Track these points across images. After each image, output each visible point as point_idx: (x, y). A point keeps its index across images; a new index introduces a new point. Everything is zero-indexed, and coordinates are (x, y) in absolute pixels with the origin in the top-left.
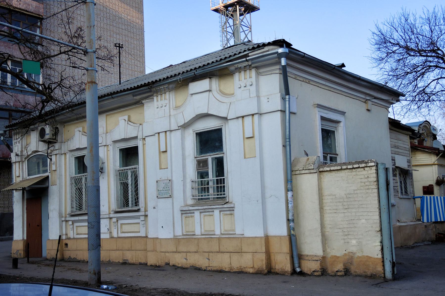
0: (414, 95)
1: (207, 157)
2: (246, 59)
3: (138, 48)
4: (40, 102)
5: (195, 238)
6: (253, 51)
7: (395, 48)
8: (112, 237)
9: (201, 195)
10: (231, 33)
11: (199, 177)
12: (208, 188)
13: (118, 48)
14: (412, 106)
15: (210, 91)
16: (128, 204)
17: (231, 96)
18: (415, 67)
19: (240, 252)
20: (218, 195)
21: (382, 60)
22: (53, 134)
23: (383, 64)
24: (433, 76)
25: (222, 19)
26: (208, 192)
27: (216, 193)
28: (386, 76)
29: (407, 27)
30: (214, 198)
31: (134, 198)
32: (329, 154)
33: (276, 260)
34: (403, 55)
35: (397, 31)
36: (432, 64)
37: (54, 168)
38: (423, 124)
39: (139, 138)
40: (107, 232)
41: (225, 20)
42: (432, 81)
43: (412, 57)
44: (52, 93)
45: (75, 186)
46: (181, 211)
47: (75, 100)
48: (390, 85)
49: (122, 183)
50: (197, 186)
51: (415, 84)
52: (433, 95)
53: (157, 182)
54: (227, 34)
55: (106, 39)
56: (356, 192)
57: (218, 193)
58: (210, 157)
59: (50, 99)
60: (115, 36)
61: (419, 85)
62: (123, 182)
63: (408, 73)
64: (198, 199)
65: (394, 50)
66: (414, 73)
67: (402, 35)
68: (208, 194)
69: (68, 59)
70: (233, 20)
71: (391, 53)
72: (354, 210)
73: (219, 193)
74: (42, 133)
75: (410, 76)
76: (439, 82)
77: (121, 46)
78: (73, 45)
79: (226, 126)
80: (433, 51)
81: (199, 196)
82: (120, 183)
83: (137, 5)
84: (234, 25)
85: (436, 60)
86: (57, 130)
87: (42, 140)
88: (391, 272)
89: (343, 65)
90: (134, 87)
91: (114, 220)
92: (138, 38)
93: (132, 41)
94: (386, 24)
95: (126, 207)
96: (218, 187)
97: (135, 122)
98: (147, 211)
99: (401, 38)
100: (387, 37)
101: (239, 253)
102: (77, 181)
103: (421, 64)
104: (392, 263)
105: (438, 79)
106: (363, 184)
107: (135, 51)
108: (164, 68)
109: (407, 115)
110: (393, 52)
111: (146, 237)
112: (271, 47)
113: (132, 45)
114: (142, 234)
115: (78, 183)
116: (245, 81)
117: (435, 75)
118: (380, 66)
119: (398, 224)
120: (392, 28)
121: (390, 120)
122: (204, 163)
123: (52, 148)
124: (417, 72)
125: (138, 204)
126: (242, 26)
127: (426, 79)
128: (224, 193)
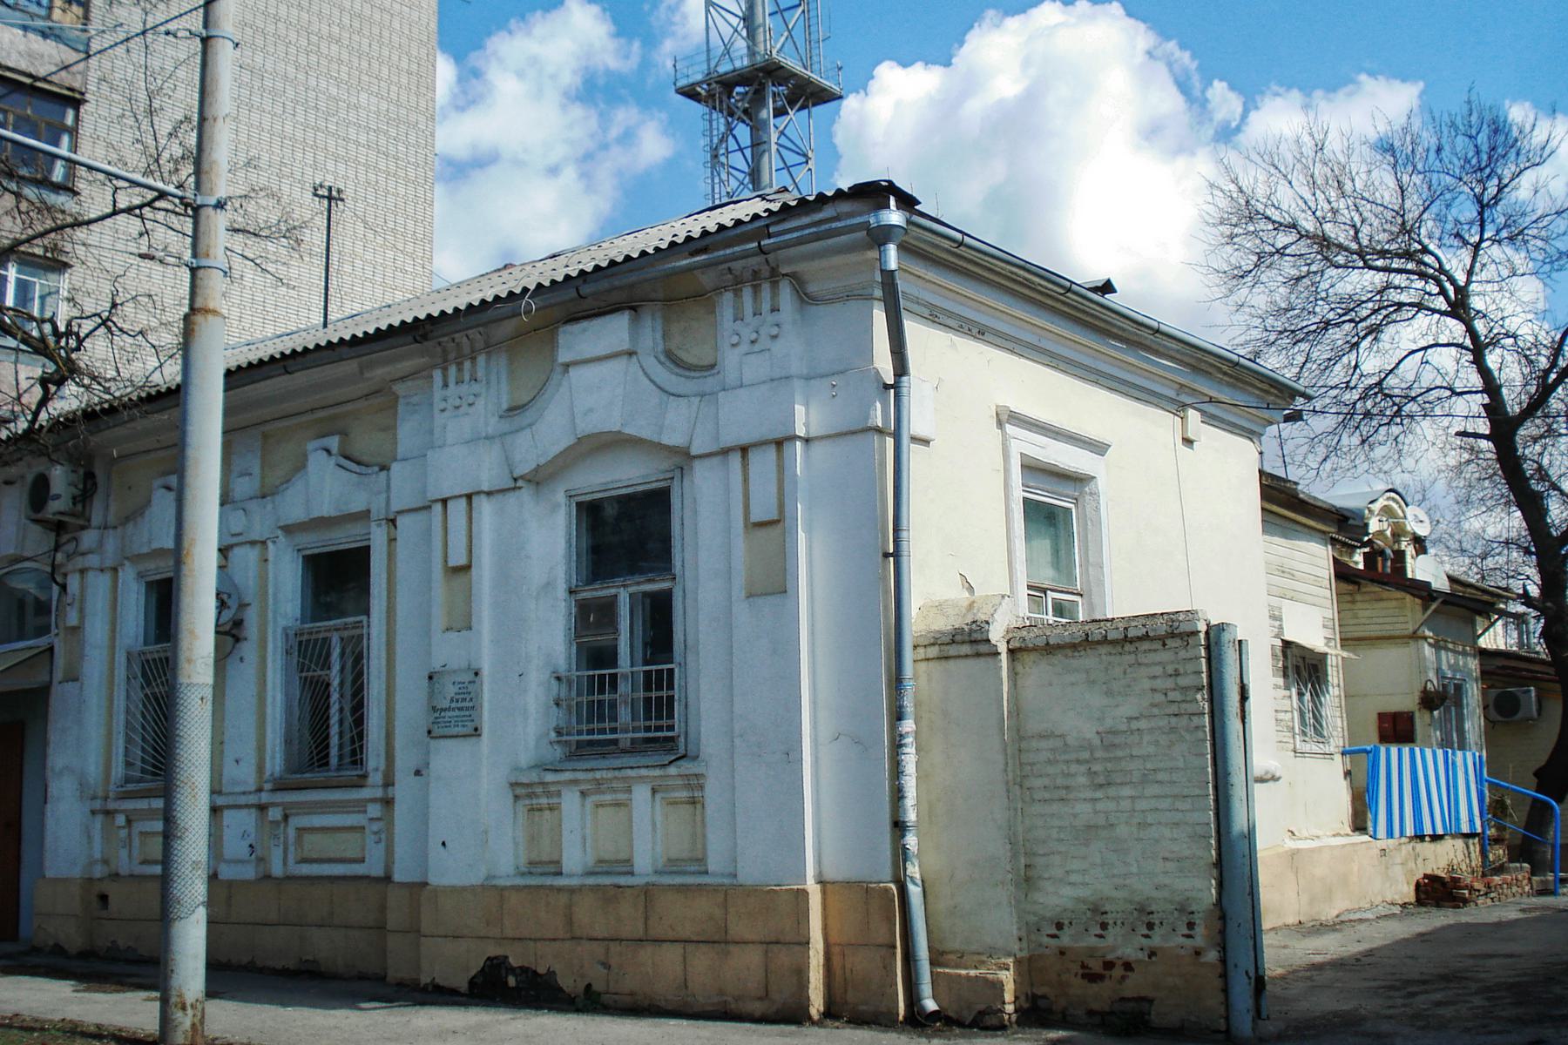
0: (1352, 401)
1: (613, 591)
2: (759, 243)
3: (410, 209)
4: (32, 381)
5: (560, 889)
6: (782, 217)
7: (1282, 239)
8: (267, 877)
9: (588, 730)
10: (743, 172)
11: (584, 664)
12: (613, 705)
13: (326, 202)
14: (1345, 436)
15: (631, 354)
16: (327, 755)
17: (706, 374)
18: (1350, 306)
19: (720, 941)
20: (648, 729)
21: (1242, 277)
22: (74, 498)
23: (1245, 291)
24: (1411, 337)
25: (711, 125)
26: (614, 718)
27: (642, 723)
28: (1255, 334)
29: (1319, 171)
30: (633, 741)
31: (347, 737)
32: (1052, 590)
33: (848, 971)
34: (1308, 261)
35: (1290, 183)
36: (1404, 298)
37: (72, 619)
38: (1381, 500)
39: (374, 516)
40: (247, 857)
41: (722, 129)
42: (1406, 353)
43: (1340, 270)
44: (78, 349)
45: (142, 688)
46: (514, 785)
47: (156, 378)
48: (1272, 362)
49: (306, 678)
50: (574, 693)
51: (1353, 363)
52: (1410, 401)
53: (430, 678)
54: (728, 173)
55: (298, 175)
56: (1135, 725)
57: (648, 723)
58: (624, 594)
59: (64, 372)
60: (330, 165)
61: (1366, 367)
62: (313, 677)
63: (1328, 323)
64: (578, 742)
65: (1280, 246)
66: (1348, 327)
67: (1308, 196)
68: (613, 725)
69: (141, 235)
70: (751, 129)
71: (1272, 254)
72: (1127, 791)
73: (653, 723)
74: (40, 492)
75: (1337, 335)
76: (1429, 359)
77: (334, 193)
78: (160, 185)
79: (685, 480)
80: (1408, 255)
81: (580, 733)
82: (301, 678)
83: (414, 67)
84: (752, 146)
85: (1419, 284)
86: (89, 483)
87: (39, 516)
88: (1248, 1011)
89: (1107, 288)
90: (366, 333)
91: (275, 814)
92: (412, 175)
93: (391, 185)
94: (1254, 157)
95: (319, 766)
96: (648, 701)
97: (365, 459)
98: (393, 785)
99: (1303, 206)
100: (1258, 201)
101: (716, 945)
102: (151, 670)
103: (1370, 295)
104: (1253, 980)
105: (1425, 348)
106: (1159, 698)
107: (400, 220)
108: (1148, 616)
109: (1328, 465)
110: (1278, 252)
111: (387, 879)
112: (845, 207)
113: (391, 199)
114: (374, 868)
115: (153, 674)
116: (755, 321)
117: (1417, 333)
118: (1234, 298)
119: (1291, 844)
120: (1272, 170)
121: (1264, 478)
122: (606, 611)
123: (70, 547)
124: (1360, 322)
125: (362, 759)
126: (781, 149)
127: (1388, 346)
128: (670, 722)
